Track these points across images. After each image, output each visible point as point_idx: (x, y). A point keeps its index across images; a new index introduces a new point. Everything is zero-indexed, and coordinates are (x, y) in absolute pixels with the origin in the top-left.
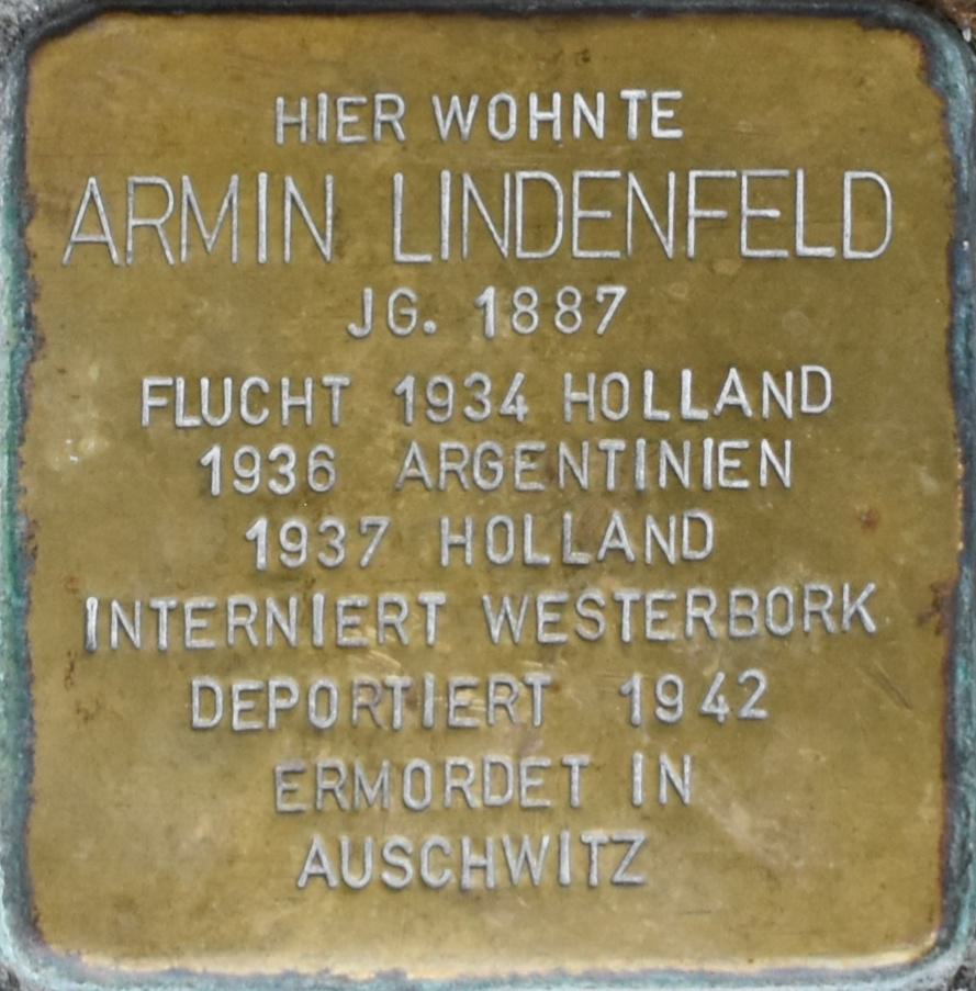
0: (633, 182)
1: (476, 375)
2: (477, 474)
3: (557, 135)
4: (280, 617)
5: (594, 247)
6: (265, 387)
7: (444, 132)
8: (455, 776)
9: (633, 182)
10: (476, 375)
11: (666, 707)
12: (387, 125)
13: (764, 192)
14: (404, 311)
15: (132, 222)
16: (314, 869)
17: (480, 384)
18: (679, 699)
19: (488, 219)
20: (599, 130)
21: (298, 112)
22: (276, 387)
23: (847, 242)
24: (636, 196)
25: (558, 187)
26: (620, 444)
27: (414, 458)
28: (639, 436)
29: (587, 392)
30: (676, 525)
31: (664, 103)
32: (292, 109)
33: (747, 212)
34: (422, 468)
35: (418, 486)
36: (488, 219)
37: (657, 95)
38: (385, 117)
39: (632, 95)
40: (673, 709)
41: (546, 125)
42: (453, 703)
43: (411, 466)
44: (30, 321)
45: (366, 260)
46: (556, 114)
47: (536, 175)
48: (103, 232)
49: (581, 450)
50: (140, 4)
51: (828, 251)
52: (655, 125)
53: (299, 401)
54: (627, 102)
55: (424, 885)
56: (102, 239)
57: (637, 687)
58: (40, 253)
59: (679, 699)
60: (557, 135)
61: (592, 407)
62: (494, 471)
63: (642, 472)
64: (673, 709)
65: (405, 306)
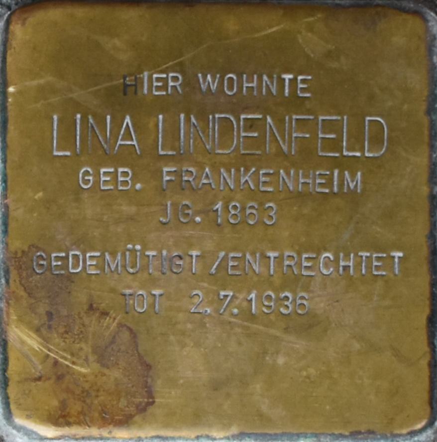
0: (269, 120)
5: (247, 149)
9: (269, 120)
13: (329, 126)
14: (86, 178)
15: (294, 135)
19: (78, 133)
20: (274, 92)
24: (270, 126)
25: (232, 119)
33: (321, 136)
36: (78, 133)
37: (300, 78)
39: (288, 77)
41: (251, 89)
44: (148, 205)
46: (254, 84)
47: (223, 116)
48: (132, 140)
53: (347, 264)
54: (284, 80)
56: (133, 143)
65: (87, 176)
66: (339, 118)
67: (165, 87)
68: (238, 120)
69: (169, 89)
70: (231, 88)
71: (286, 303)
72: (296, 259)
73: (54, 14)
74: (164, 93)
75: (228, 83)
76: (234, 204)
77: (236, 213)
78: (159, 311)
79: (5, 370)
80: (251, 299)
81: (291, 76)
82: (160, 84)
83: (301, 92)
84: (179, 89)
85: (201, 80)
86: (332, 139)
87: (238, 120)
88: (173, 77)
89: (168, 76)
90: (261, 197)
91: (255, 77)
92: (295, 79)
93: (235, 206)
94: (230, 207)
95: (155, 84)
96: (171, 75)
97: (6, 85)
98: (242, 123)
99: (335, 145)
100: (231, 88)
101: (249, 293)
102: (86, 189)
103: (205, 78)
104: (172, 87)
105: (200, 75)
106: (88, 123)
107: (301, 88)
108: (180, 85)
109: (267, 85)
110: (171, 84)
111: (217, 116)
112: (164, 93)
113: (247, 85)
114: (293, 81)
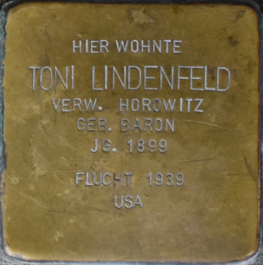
3: (149, 51)
8: (76, 103)
12: (104, 48)
13: (197, 72)
18: (162, 179)
20: (160, 51)
21: (79, 45)
27: (138, 199)
30: (88, 44)
31: (177, 44)
32: (77, 44)
34: (140, 201)
35: (139, 207)
38: (103, 46)
42: (88, 125)
43: (137, 201)
45: (148, 177)
50: (47, 264)
51: (214, 89)
52: (174, 49)
55: (95, 185)
57: (131, 142)
59: (162, 179)
60: (149, 51)
66: (203, 67)
67: (98, 49)
68: (142, 69)
69: (101, 49)
70: (135, 48)
73: (31, 10)
75: (133, 45)
76: (152, 140)
77: (141, 145)
81: (170, 41)
82: (178, 47)
83: (176, 50)
84: (106, 49)
87: (142, 69)
88: (103, 42)
89: (100, 42)
90: (87, 122)
91: (80, 42)
92: (172, 42)
93: (153, 142)
94: (138, 142)
95: (92, 47)
98: (145, 71)
99: (199, 84)
100: (135, 48)
105: (117, 41)
107: (176, 48)
108: (107, 47)
109: (156, 47)
110: (102, 46)
113: (93, 47)
114: (171, 44)
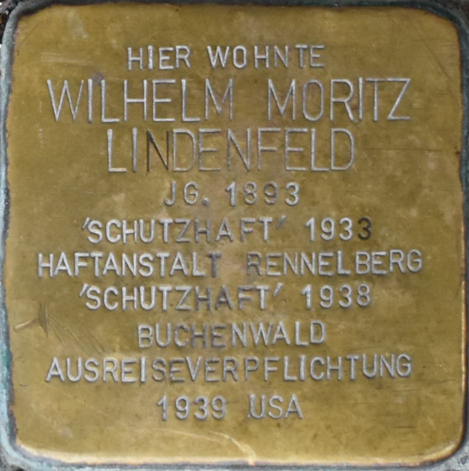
1: (291, 184)
2: (409, 264)
4: (308, 261)
6: (116, 292)
7: (214, 63)
10: (291, 184)
11: (326, 233)
16: (224, 233)
17: (293, 187)
22: (121, 291)
23: (340, 266)
26: (100, 254)
28: (51, 253)
29: (133, 228)
34: (183, 265)
40: (329, 234)
49: (192, 257)
58: (217, 278)
61: (136, 235)
62: (418, 263)
63: (41, 271)
64: (329, 234)
71: (202, 407)
72: (151, 342)
74: (172, 67)
78: (276, 296)
79: (410, 467)
80: (230, 190)
82: (167, 58)
85: (210, 52)
86: (170, 70)
88: (180, 50)
96: (178, 47)
97: (246, 466)
101: (228, 183)
102: (236, 67)
103: (214, 49)
104: (133, 61)
106: (175, 257)
110: (178, 56)
111: (154, 82)
112: (172, 67)
